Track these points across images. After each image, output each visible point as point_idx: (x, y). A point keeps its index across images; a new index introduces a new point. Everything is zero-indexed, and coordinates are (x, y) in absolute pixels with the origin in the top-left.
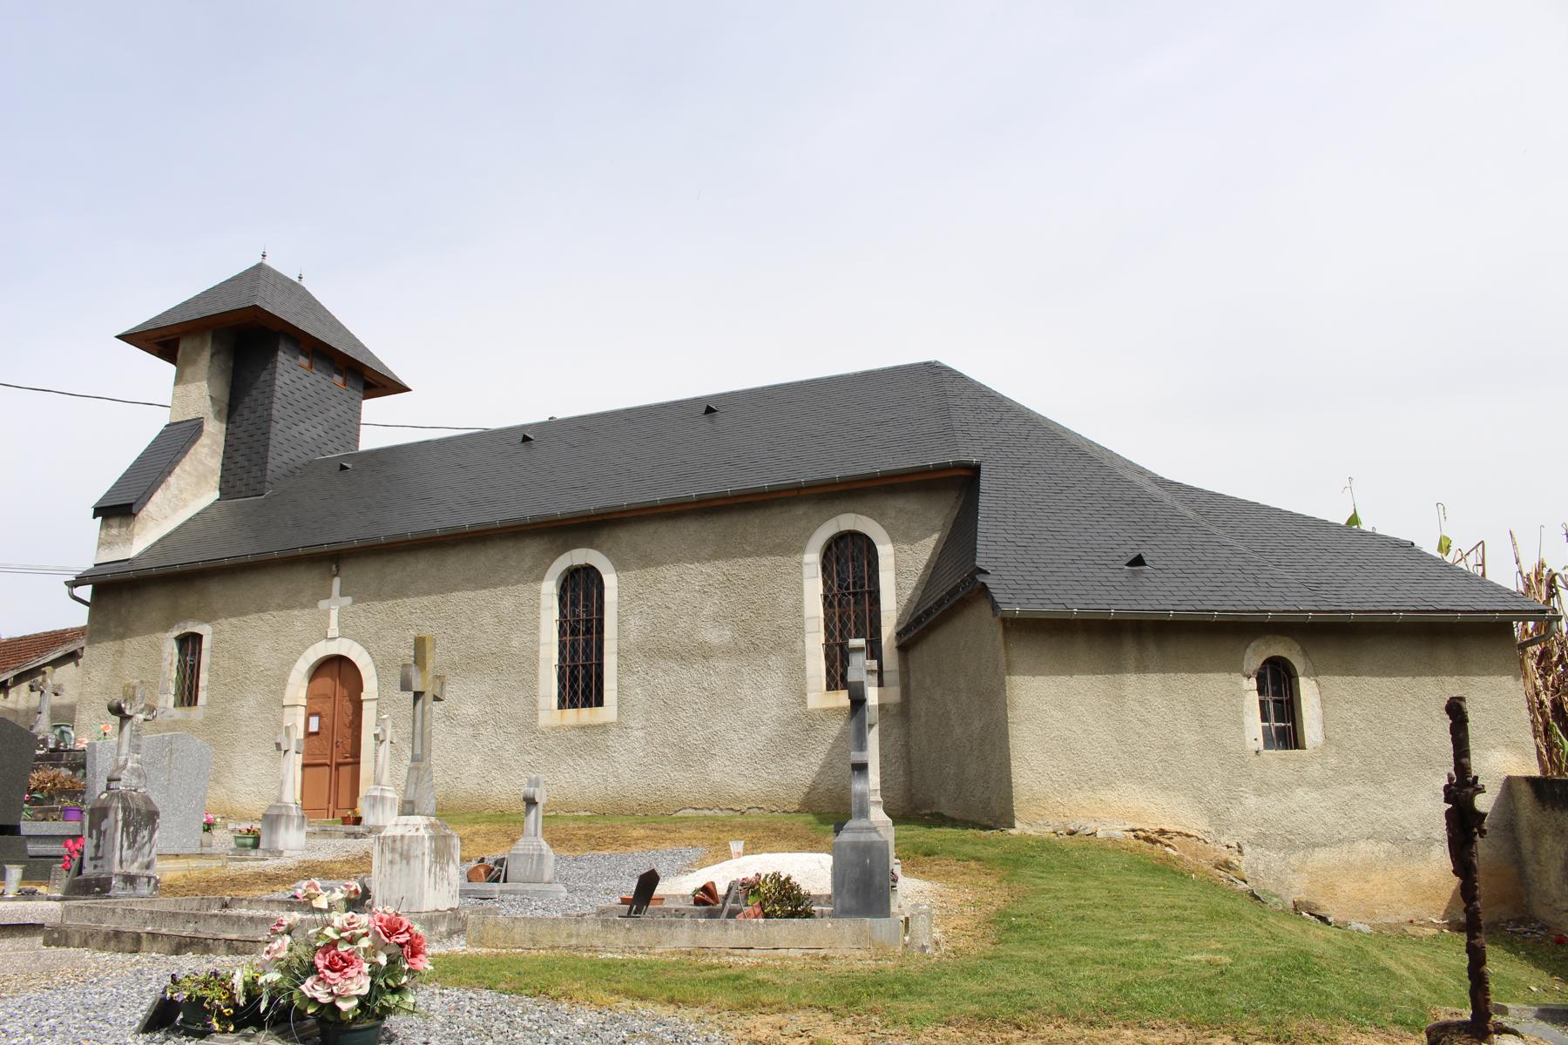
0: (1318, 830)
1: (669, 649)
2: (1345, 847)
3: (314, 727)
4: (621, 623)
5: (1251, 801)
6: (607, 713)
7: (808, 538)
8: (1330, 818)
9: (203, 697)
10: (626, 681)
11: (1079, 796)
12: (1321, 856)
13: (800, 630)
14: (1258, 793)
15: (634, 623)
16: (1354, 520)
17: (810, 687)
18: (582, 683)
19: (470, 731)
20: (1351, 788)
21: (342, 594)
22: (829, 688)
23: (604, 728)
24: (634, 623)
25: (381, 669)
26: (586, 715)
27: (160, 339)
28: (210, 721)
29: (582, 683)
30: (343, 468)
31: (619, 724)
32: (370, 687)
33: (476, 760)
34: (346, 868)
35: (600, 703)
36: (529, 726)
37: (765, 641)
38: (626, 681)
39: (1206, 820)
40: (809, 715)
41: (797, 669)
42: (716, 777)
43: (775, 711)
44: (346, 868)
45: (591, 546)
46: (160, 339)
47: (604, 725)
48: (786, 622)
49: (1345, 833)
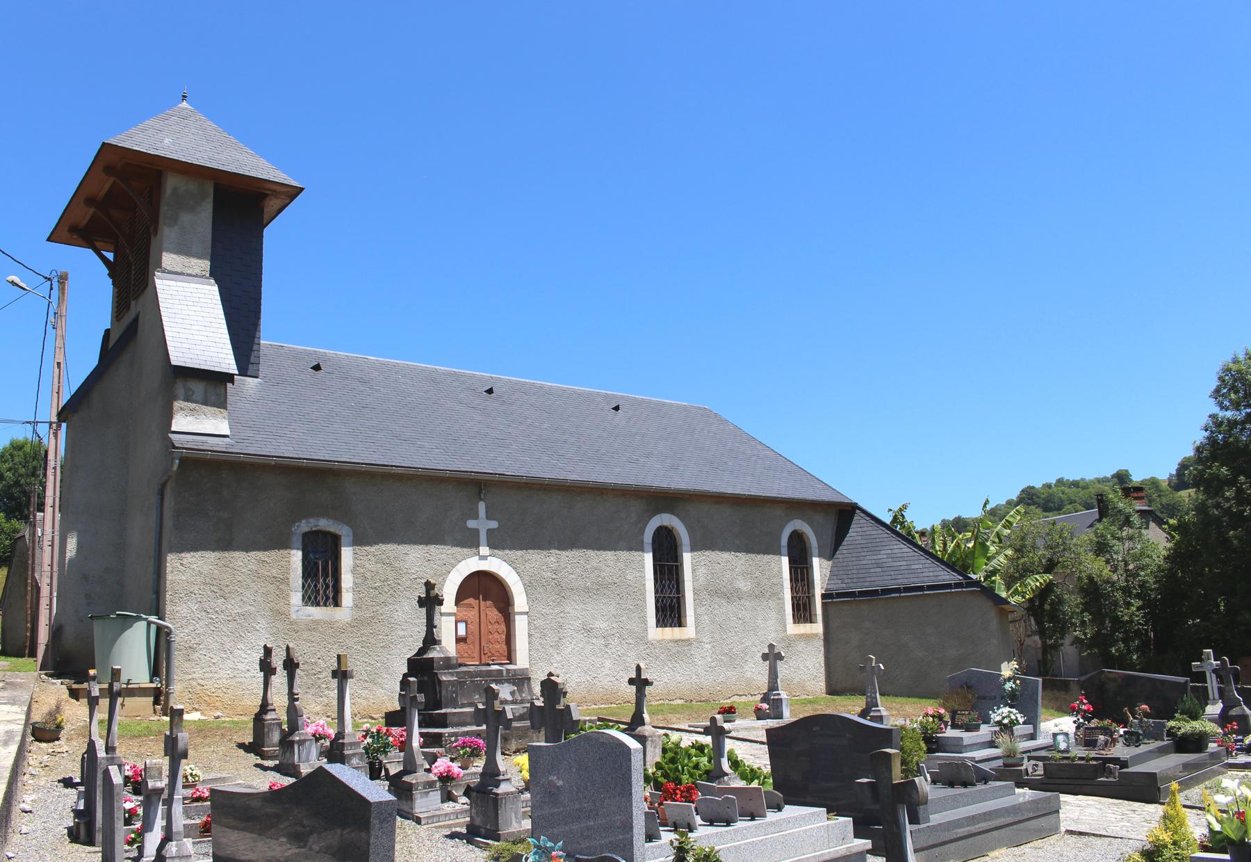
1: (717, 592)
3: (462, 631)
4: (694, 571)
6: (689, 631)
10: (700, 611)
13: (644, 594)
16: (322, 582)
19: (602, 641)
21: (488, 517)
23: (688, 642)
24: (702, 571)
25: (529, 587)
31: (696, 640)
32: (520, 601)
33: (608, 664)
34: (271, 809)
36: (642, 638)
37: (764, 593)
38: (700, 611)
40: (788, 637)
42: (748, 675)
44: (271, 809)
45: (673, 513)
47: (688, 640)
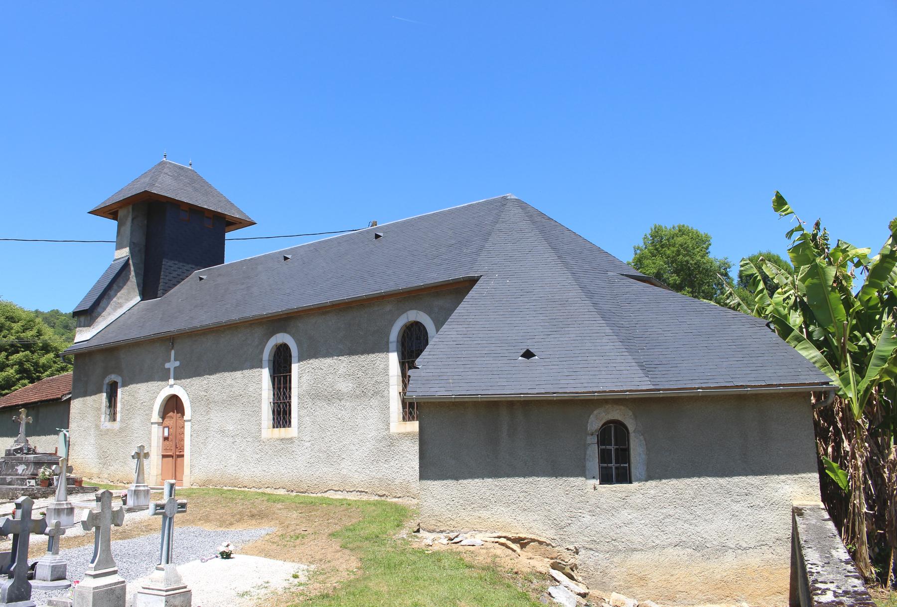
0: (637, 539)
1: (323, 395)
2: (657, 552)
3: (166, 434)
5: (587, 519)
7: (392, 325)
8: (647, 532)
9: (118, 416)
11: (463, 514)
12: (637, 556)
14: (592, 513)
15: (305, 377)
17: (391, 419)
18: (282, 415)
19: (231, 440)
20: (664, 511)
22: (404, 419)
23: (291, 440)
26: (282, 432)
27: (110, 211)
28: (122, 430)
29: (282, 415)
30: (286, 258)
35: (290, 426)
36: (257, 438)
37: (371, 392)
39: (553, 531)
41: (385, 408)
42: (344, 472)
43: (374, 433)
45: (285, 331)
46: (110, 211)
47: (291, 439)
48: (379, 379)
49: (657, 542)
